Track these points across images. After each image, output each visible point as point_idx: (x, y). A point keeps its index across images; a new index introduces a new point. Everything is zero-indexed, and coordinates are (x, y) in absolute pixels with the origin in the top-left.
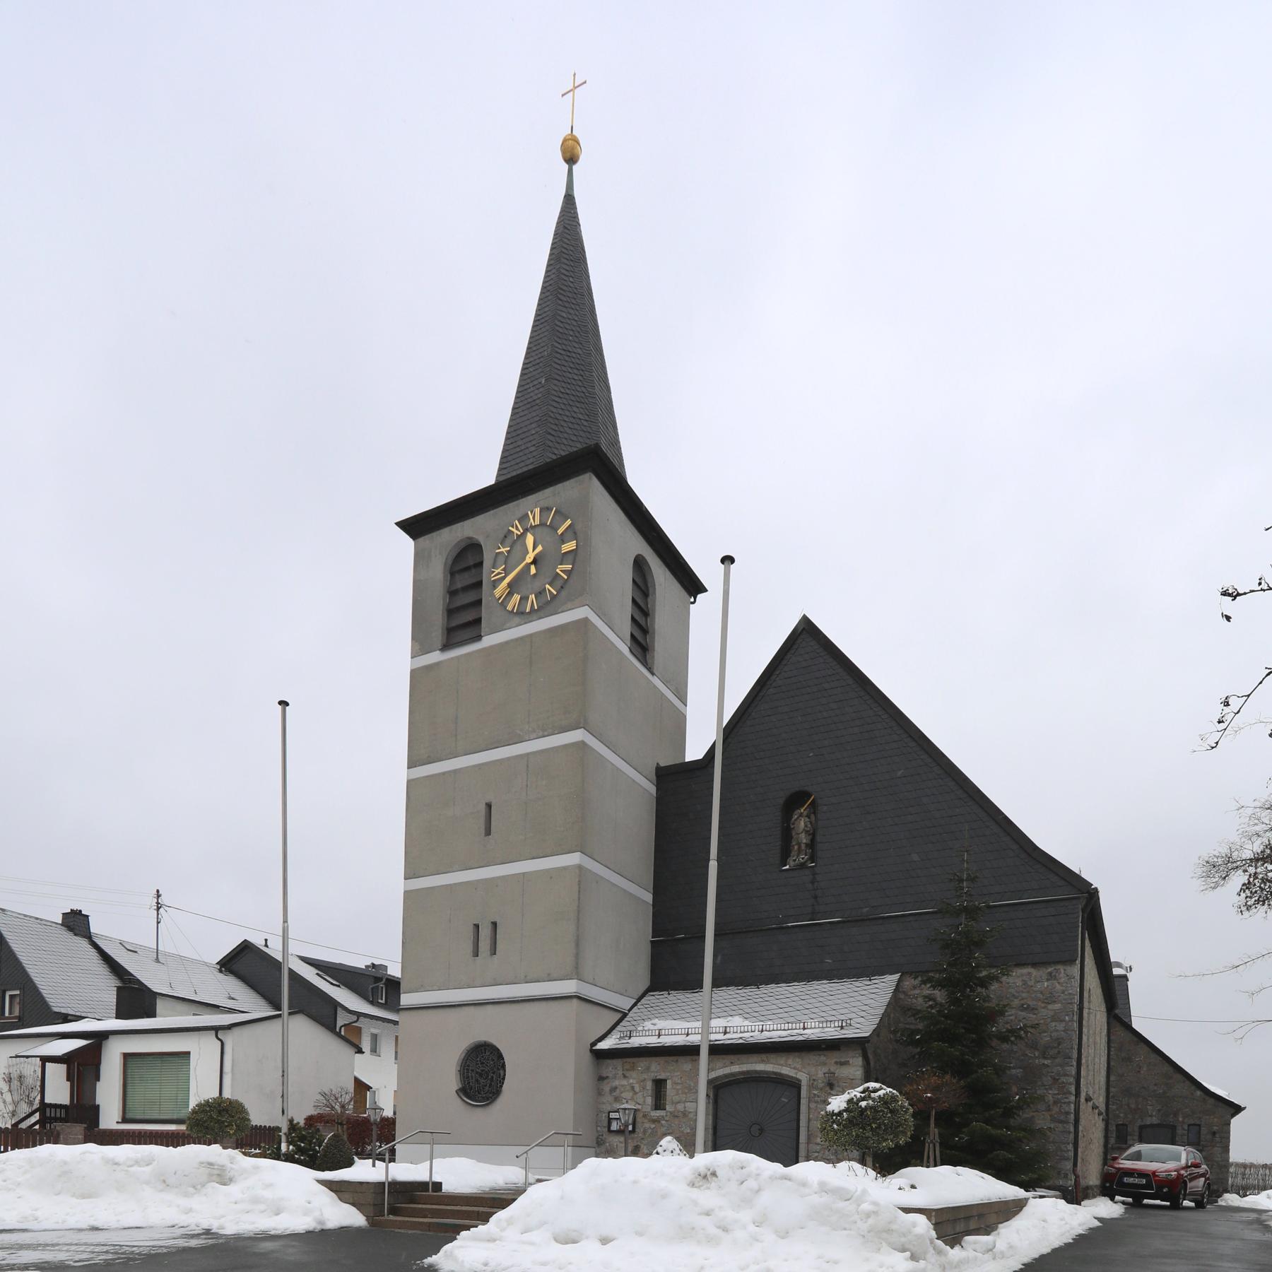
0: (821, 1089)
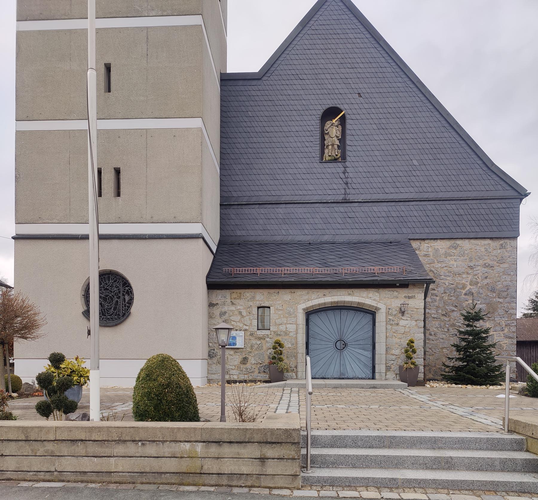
0: (395, 315)
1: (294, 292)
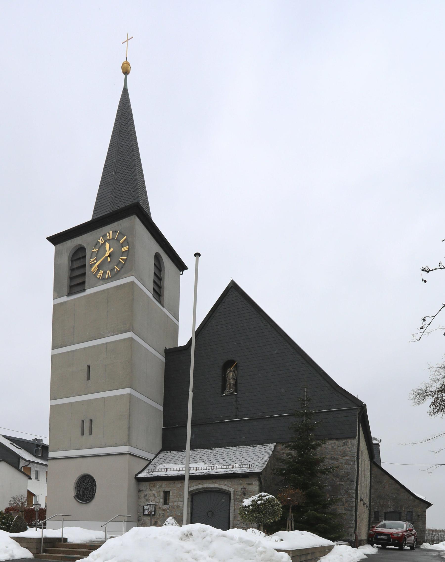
0: (240, 496)
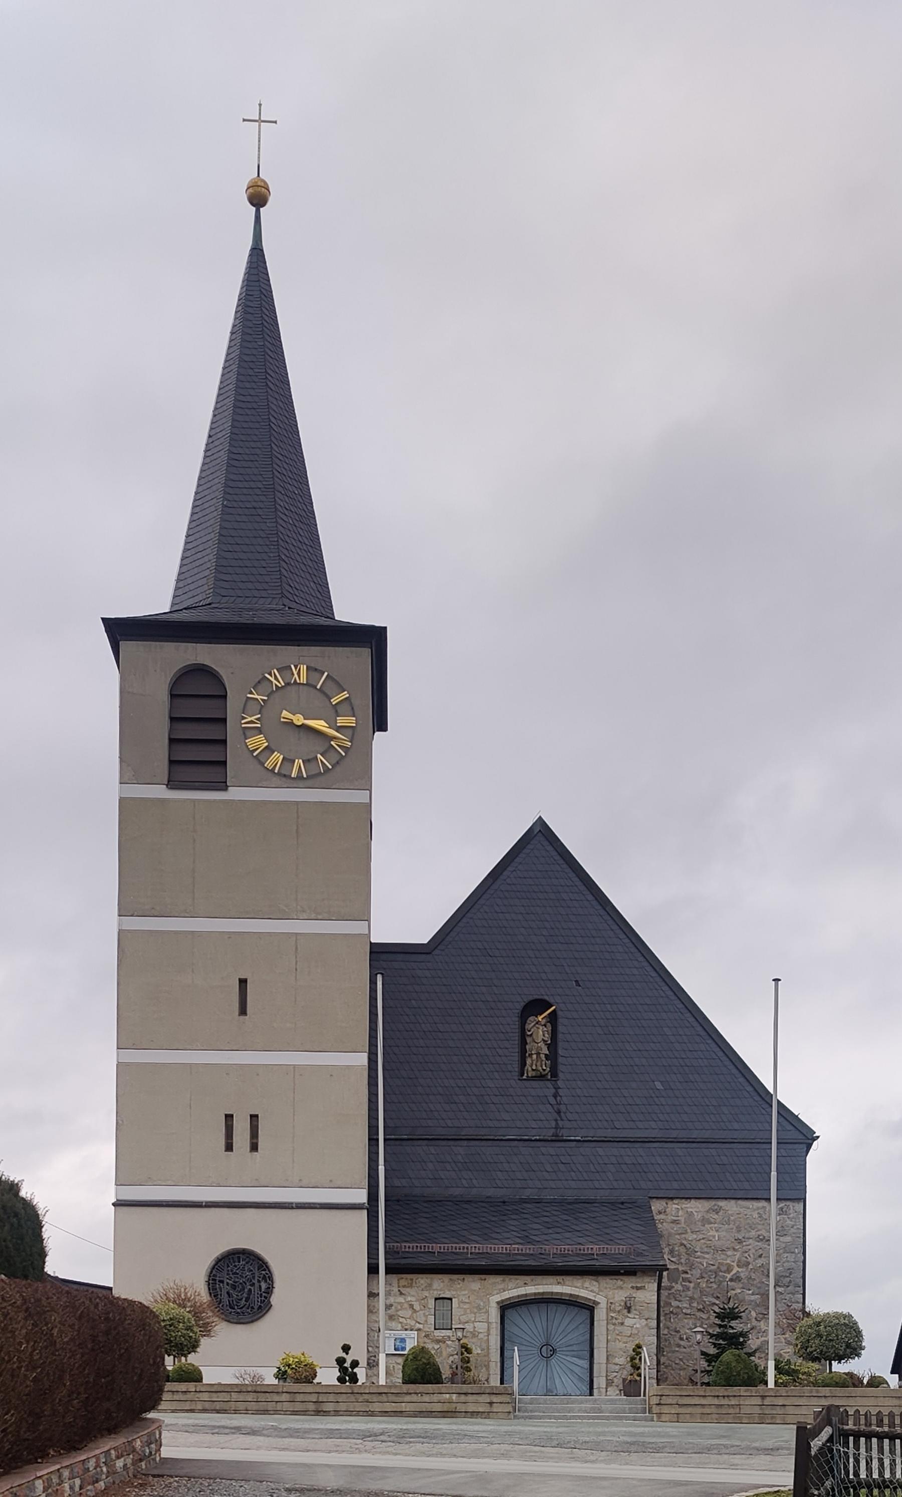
0: (619, 1312)
1: (485, 1279)
